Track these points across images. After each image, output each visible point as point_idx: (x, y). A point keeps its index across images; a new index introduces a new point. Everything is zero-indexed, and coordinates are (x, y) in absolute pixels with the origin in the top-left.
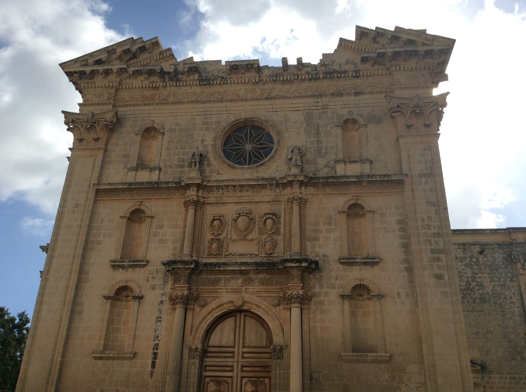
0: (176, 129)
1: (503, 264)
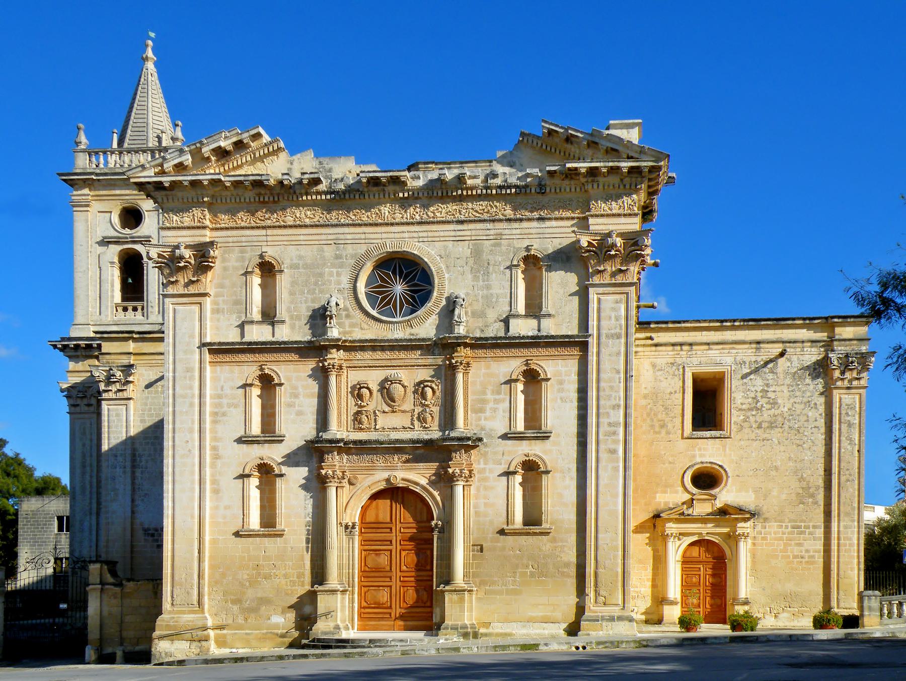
1: (814, 371)
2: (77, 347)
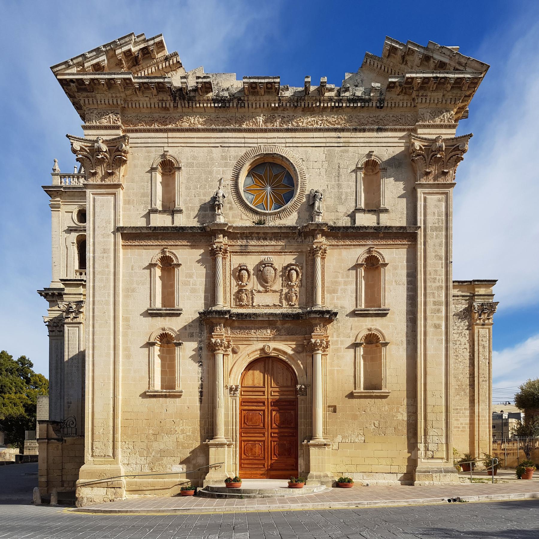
2: (53, 294)
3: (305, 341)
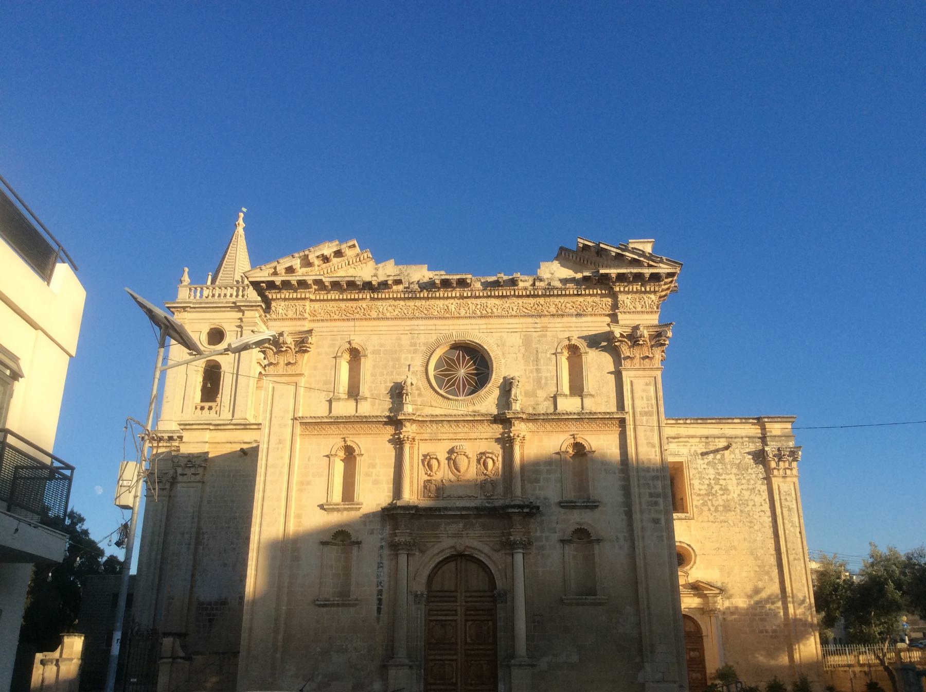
0: (380, 350)
3: (503, 538)
